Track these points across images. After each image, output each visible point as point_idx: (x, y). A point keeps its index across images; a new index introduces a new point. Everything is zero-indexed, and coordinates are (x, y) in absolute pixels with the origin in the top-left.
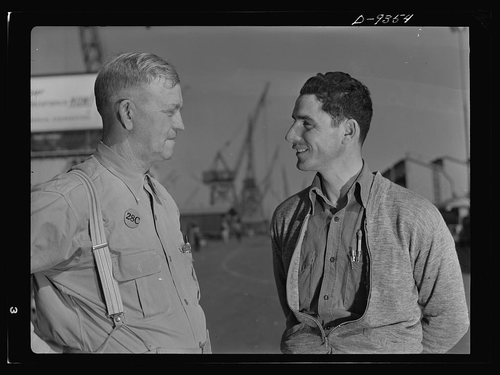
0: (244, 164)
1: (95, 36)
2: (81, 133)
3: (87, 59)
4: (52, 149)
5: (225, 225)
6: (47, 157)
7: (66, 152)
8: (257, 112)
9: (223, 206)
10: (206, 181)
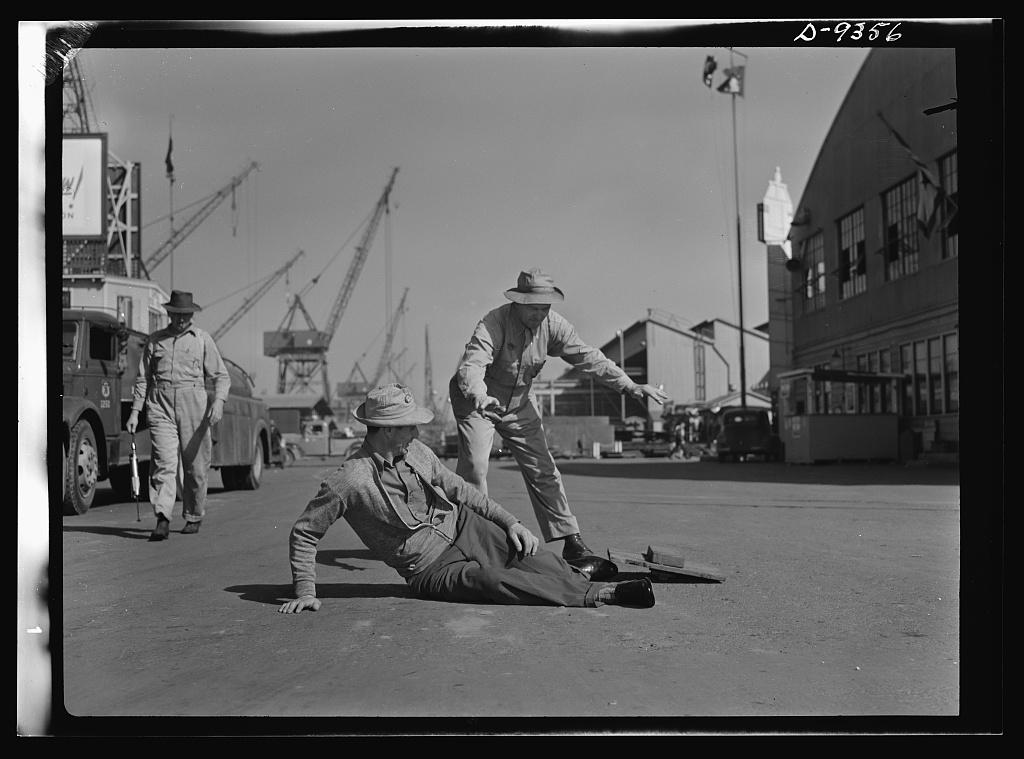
10: (270, 352)
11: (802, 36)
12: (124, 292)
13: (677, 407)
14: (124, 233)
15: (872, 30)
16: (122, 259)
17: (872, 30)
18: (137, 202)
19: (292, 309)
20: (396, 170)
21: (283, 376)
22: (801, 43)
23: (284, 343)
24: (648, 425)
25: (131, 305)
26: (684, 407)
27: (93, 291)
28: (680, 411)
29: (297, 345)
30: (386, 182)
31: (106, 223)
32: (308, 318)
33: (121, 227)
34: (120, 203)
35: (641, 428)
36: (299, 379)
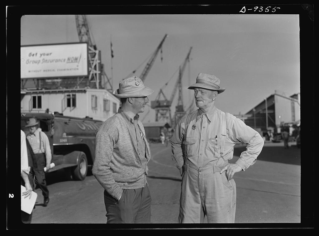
0: (177, 96)
1: (85, 20)
2: (75, 78)
3: (80, 33)
4: (57, 88)
5: (162, 133)
6: (53, 92)
7: (65, 89)
8: (185, 65)
9: (162, 122)
10: (153, 107)
11: (241, 11)
12: (94, 94)
13: (285, 124)
14: (96, 74)
15: (266, 9)
16: (95, 83)
17: (266, 9)
18: (100, 63)
19: (159, 94)
20: (191, 48)
21: (157, 115)
22: (241, 13)
23: (157, 104)
24: (276, 130)
25: (96, 98)
26: (287, 124)
27: (83, 94)
28: (286, 125)
29: (161, 105)
30: (188, 52)
31: (89, 72)
32: (164, 96)
33: (95, 72)
34: (94, 65)
35: (273, 131)
36: (162, 116)
